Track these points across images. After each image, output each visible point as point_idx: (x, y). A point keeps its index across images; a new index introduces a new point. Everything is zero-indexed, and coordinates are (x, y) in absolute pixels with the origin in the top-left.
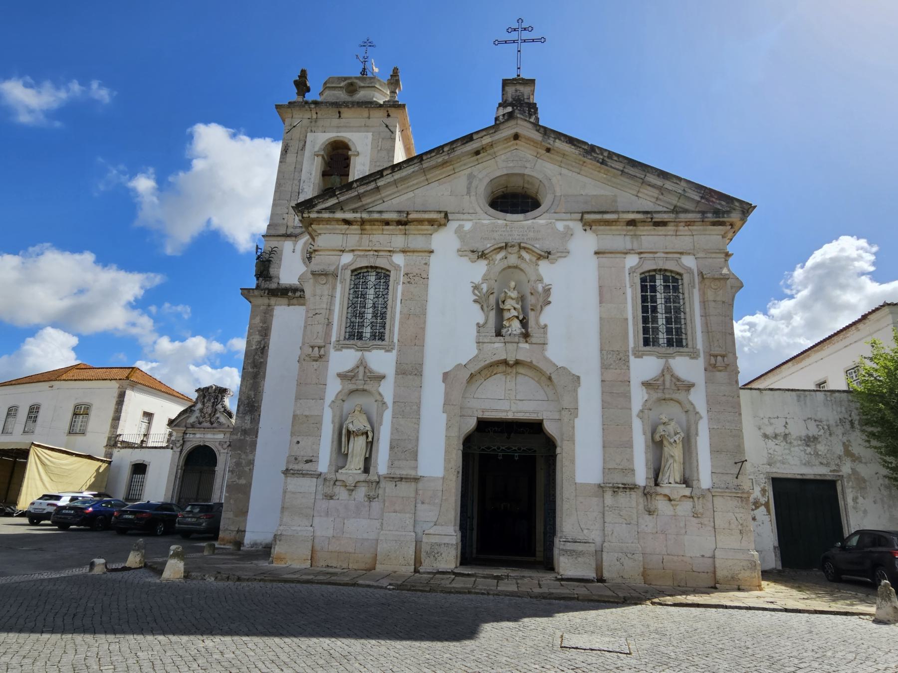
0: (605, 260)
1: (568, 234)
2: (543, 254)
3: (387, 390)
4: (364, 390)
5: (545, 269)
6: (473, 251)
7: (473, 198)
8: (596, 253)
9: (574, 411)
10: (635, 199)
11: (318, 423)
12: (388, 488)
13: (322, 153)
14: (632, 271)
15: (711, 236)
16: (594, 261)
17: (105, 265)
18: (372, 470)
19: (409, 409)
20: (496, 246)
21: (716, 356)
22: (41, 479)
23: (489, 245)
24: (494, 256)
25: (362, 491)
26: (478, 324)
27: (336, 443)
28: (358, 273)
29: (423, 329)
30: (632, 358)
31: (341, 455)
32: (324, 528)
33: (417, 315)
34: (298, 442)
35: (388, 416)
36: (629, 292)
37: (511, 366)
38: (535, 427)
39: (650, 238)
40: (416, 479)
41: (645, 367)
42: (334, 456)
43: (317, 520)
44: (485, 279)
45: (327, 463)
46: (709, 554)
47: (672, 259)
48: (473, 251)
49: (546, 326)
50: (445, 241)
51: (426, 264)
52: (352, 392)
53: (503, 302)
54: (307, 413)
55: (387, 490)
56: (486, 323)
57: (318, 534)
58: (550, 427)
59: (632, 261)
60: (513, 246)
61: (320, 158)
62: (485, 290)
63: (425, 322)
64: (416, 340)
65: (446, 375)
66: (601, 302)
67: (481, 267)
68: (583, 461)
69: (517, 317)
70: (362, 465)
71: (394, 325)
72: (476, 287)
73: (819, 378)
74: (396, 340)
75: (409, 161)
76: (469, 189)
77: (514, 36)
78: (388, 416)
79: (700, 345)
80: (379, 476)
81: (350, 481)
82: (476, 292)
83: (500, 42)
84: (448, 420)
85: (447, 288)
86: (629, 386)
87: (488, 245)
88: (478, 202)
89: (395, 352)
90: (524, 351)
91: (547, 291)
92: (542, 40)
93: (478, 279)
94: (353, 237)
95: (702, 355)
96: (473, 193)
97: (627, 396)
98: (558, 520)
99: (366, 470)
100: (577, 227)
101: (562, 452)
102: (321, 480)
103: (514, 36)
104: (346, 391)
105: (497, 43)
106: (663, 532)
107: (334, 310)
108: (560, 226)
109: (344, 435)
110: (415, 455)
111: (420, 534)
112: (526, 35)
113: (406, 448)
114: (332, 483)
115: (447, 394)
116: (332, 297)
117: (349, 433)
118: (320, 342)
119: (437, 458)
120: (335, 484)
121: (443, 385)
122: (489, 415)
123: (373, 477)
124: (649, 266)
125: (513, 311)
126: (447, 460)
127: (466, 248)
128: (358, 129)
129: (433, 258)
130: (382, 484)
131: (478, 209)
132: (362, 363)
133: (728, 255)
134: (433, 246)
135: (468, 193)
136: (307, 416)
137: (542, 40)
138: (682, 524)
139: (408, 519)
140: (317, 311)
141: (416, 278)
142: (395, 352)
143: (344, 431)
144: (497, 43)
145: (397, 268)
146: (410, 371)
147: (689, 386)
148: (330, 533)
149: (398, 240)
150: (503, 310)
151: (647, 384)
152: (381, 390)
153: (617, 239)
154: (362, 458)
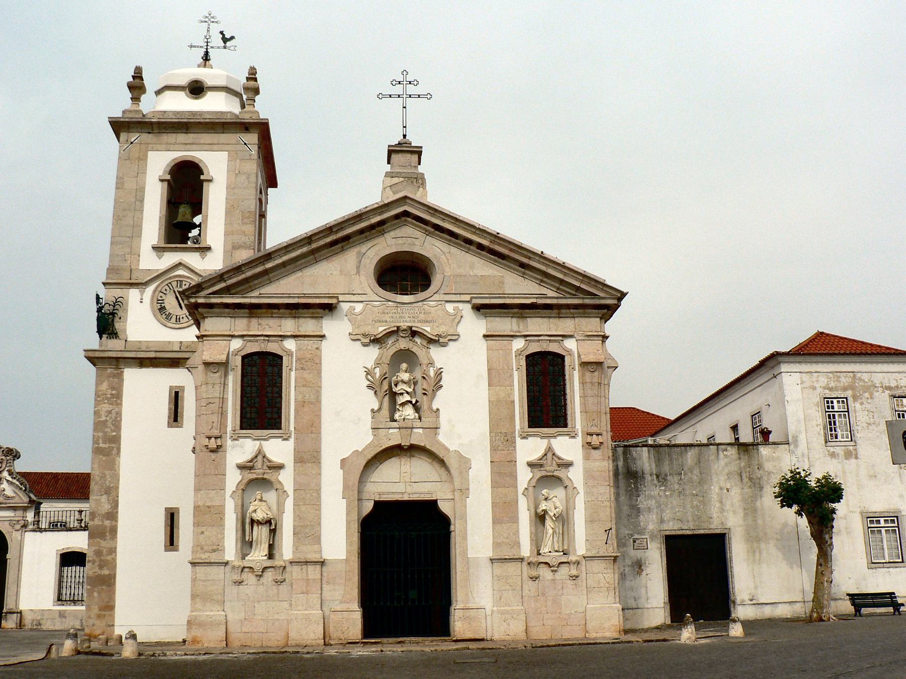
0: (492, 343)
1: (458, 318)
2: (434, 338)
3: (286, 478)
4: (263, 479)
5: (436, 353)
7: (363, 278)
8: (485, 336)
9: (464, 491)
10: (519, 287)
11: (220, 513)
12: (295, 572)
13: (168, 177)
14: (519, 353)
15: (591, 324)
16: (483, 344)
18: (277, 556)
19: (308, 496)
21: (591, 435)
25: (269, 576)
26: (372, 410)
27: (240, 532)
28: (248, 360)
29: (319, 416)
30: (518, 440)
31: (246, 544)
32: (234, 614)
33: (312, 405)
34: (203, 533)
35: (289, 504)
36: (516, 373)
37: (406, 450)
38: (431, 506)
39: (537, 325)
40: (322, 563)
41: (530, 448)
42: (239, 544)
43: (227, 605)
44: (378, 364)
45: (234, 551)
46: (582, 609)
47: (555, 341)
49: (438, 410)
50: (336, 330)
51: (317, 349)
52: (251, 481)
53: (396, 385)
54: (209, 504)
55: (294, 574)
56: (380, 409)
57: (230, 618)
58: (445, 507)
59: (518, 344)
61: (166, 184)
62: (378, 375)
63: (320, 409)
64: (311, 428)
65: (343, 461)
66: (490, 385)
67: (373, 352)
68: (475, 540)
70: (266, 552)
71: (289, 415)
73: (710, 433)
74: (292, 428)
76: (358, 268)
77: (398, 89)
78: (289, 504)
79: (578, 426)
80: (284, 561)
81: (258, 568)
82: (369, 377)
83: (384, 96)
84: (348, 506)
85: (338, 376)
86: (515, 465)
87: (381, 329)
88: (366, 282)
89: (292, 440)
90: (418, 437)
91: (439, 374)
92: (428, 96)
93: (370, 365)
94: (240, 325)
95: (580, 434)
96: (362, 272)
97: (513, 476)
98: (453, 591)
99: (271, 556)
100: (467, 309)
101: (456, 528)
102: (228, 568)
103: (398, 89)
104: (245, 481)
105: (380, 96)
106: (543, 594)
107: (227, 399)
108: (450, 307)
109: (247, 524)
110: (317, 540)
111: (327, 613)
112: (411, 89)
113: (308, 530)
114: (240, 570)
115: (345, 479)
116: (225, 385)
117: (252, 521)
118: (216, 432)
119: (338, 541)
120: (242, 571)
121: (342, 471)
122: (385, 498)
123: (277, 562)
124: (535, 348)
125: (405, 395)
126: (349, 543)
127: (357, 331)
128: (211, 147)
129: (324, 344)
130: (288, 569)
131: (368, 291)
132: (260, 453)
133: (605, 337)
134: (325, 332)
135: (358, 272)
136: (209, 507)
137: (428, 96)
138: (560, 587)
139: (315, 599)
140: (211, 400)
141: (309, 364)
142: (292, 440)
143: (248, 521)
144: (380, 96)
145: (290, 353)
146: (309, 458)
147: (568, 465)
148: (242, 615)
149: (288, 325)
150: (395, 393)
151: (531, 465)
152: (280, 478)
153: (505, 325)
154: (267, 546)
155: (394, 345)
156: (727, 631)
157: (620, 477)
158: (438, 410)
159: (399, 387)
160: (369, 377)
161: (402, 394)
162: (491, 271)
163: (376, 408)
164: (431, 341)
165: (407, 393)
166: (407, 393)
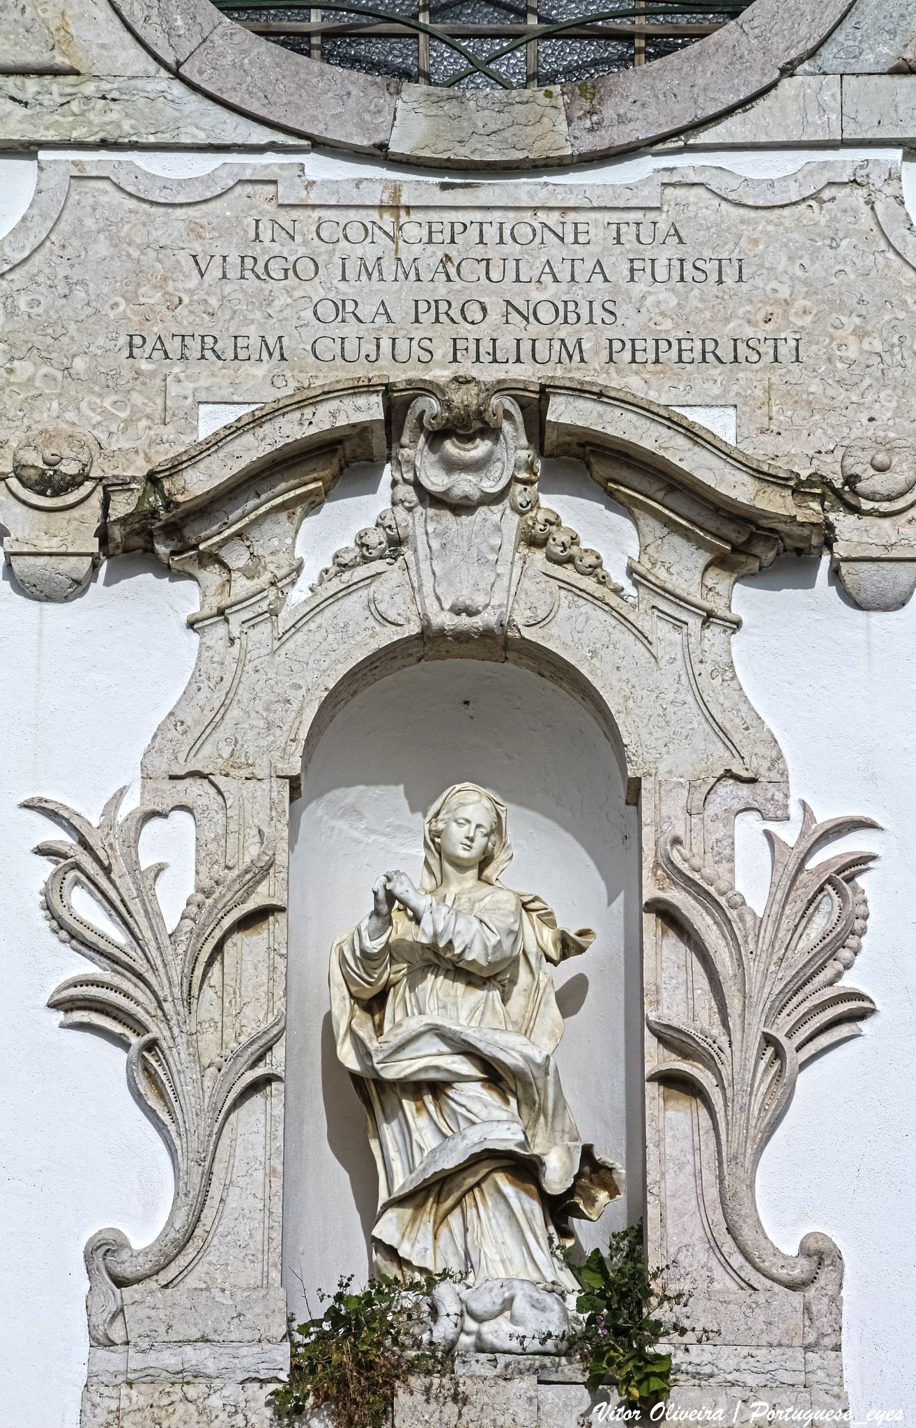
6: (50, 483)
17: (459, 515)
20: (291, 430)
22: (127, 995)
23: (211, 421)
24: (271, 539)
26: (103, 1251)
44: (183, 776)
48: (50, 483)
49: (821, 1256)
56: (183, 1241)
60: (468, 425)
62: (173, 899)
69: (524, 1168)
72: (82, 857)
75: (309, 8)
82: (84, 906)
87: (206, 422)
125: (474, 1095)
155: (335, 580)
156: (526, 21)
157: (691, 141)
158: (821, 1256)
159: (402, 1017)
160: (84, 906)
161: (434, 1088)
162: (614, 26)
163: (143, 1236)
164: (759, 546)
165: (496, 1075)
166: (496, 1075)
